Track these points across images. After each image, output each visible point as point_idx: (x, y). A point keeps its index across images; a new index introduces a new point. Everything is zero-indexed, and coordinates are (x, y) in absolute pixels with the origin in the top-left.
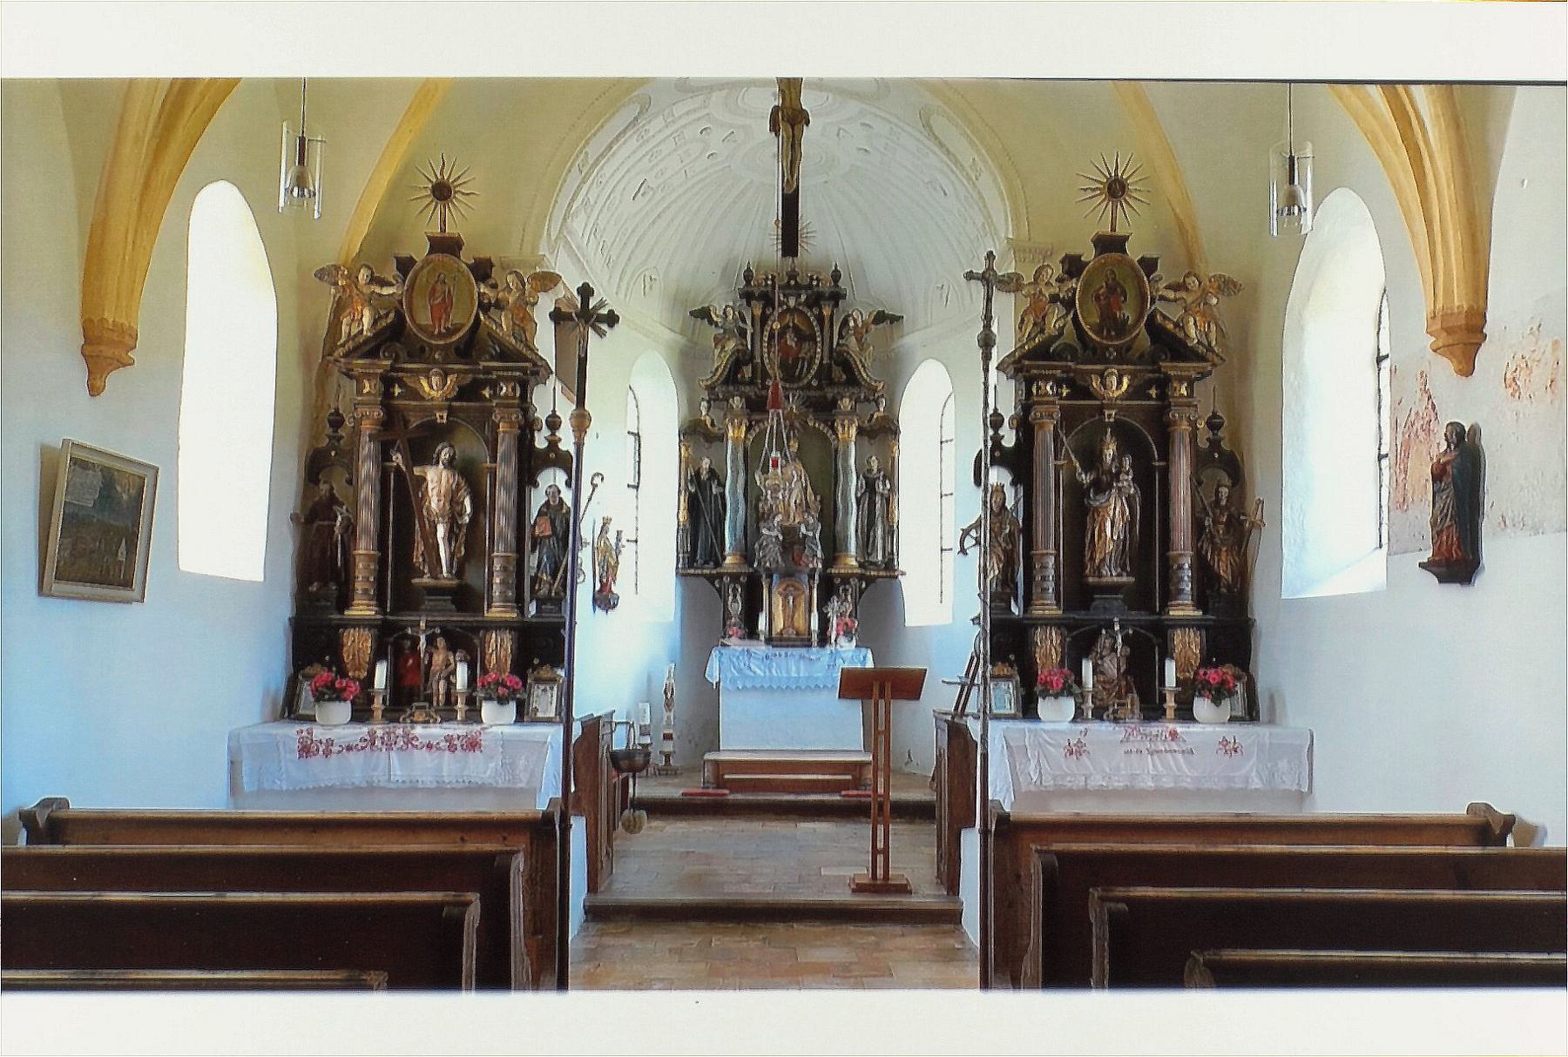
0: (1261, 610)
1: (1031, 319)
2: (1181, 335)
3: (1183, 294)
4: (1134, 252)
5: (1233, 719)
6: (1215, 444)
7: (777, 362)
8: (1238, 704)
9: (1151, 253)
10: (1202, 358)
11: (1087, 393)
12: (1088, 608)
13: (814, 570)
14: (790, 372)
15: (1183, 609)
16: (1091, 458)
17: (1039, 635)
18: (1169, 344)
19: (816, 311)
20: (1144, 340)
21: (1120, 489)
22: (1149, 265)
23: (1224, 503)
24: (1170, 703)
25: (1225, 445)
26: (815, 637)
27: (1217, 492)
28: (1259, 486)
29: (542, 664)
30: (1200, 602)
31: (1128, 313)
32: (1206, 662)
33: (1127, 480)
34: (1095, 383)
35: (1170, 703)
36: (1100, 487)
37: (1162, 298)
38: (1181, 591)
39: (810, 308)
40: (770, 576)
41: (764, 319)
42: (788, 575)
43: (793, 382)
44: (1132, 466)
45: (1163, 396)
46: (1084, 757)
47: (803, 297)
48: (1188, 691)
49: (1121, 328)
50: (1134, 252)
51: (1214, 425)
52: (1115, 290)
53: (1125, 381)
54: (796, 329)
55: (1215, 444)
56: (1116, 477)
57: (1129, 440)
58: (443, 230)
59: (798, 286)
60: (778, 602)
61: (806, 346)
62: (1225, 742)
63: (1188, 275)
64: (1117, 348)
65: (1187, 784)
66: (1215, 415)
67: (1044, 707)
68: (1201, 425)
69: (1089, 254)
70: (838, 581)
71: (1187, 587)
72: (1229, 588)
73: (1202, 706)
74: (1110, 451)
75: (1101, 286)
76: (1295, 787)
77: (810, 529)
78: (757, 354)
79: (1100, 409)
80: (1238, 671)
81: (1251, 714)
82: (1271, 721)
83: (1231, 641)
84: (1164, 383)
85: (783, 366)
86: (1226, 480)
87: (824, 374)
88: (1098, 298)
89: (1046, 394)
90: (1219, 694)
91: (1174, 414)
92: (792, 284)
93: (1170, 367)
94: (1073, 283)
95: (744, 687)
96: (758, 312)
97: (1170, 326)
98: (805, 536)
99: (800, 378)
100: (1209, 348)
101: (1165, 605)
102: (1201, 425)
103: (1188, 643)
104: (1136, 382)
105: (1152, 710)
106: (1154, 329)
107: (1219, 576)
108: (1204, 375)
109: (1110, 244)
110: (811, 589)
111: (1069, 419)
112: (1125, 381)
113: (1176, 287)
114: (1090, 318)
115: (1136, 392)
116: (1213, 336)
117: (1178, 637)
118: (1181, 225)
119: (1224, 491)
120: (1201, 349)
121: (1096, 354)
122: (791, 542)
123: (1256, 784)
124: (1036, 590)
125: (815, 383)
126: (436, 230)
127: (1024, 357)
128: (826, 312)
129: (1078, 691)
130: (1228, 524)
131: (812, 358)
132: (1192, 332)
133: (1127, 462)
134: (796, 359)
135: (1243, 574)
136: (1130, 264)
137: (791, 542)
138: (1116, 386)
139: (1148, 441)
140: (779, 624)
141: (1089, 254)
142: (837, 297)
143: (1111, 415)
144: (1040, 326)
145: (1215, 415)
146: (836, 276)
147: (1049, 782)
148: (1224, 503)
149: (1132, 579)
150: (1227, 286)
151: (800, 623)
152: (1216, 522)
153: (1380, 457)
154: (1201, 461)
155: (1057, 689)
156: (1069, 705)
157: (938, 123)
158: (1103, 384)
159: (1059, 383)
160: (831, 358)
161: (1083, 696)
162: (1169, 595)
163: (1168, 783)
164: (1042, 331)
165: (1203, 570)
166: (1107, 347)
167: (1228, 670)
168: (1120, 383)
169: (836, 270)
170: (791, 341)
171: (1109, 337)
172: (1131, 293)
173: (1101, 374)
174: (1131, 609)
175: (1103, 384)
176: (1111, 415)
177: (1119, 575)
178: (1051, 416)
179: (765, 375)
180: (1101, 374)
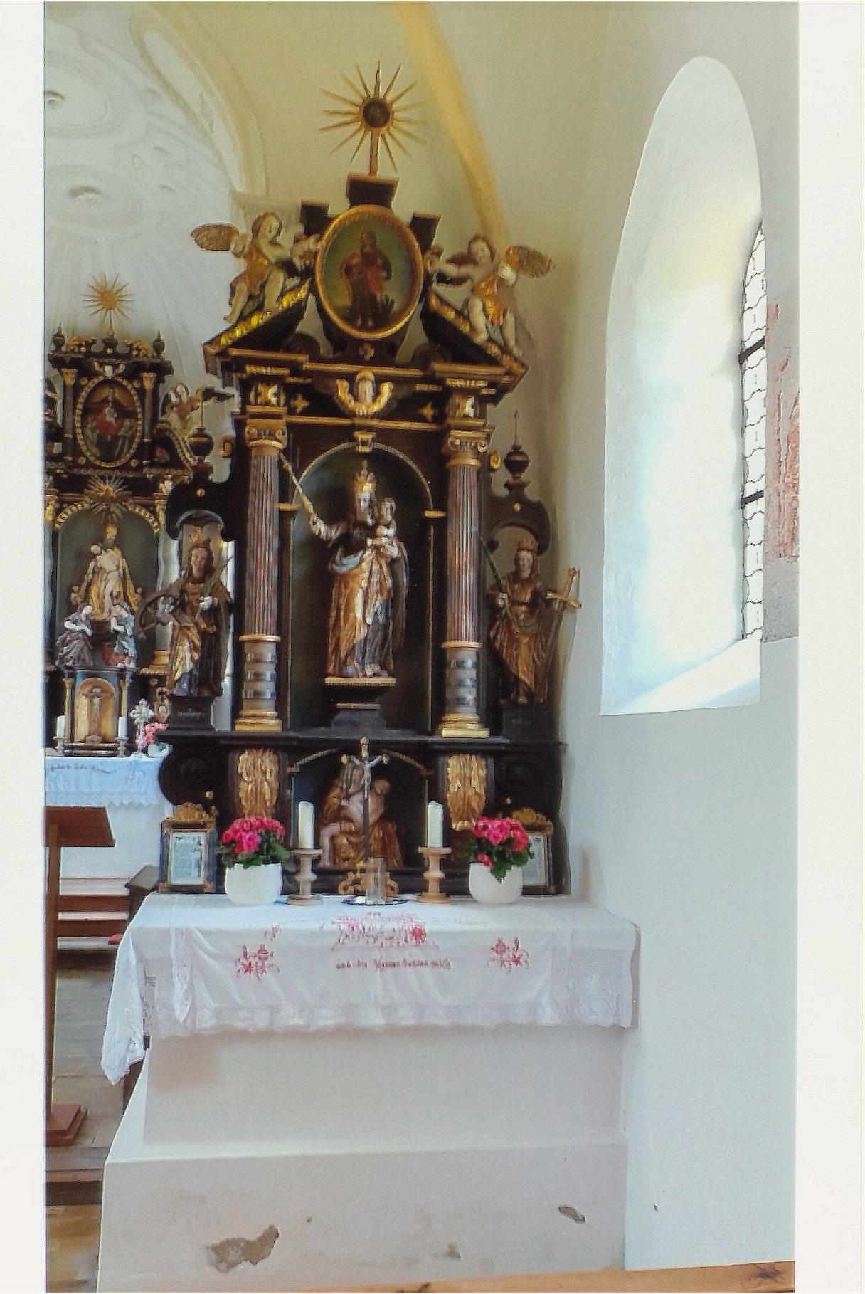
0: (576, 729)
1: (243, 288)
2: (466, 328)
3: (466, 270)
4: (403, 207)
5: (528, 891)
6: (516, 489)
7: (92, 436)
8: (536, 869)
9: (426, 210)
10: (493, 361)
11: (325, 404)
12: (328, 725)
13: (123, 670)
14: (108, 449)
15: (464, 725)
16: (336, 503)
17: (245, 762)
18: (449, 340)
19: (137, 385)
20: (417, 336)
21: (377, 549)
22: (423, 226)
23: (526, 574)
24: (434, 873)
25: (531, 493)
26: (121, 748)
27: (517, 560)
28: (573, 551)
29: (517, 806)
30: (491, 717)
31: (391, 291)
32: (491, 811)
33: (387, 533)
34: (342, 389)
35: (434, 873)
36: (351, 545)
37: (442, 278)
38: (460, 701)
39: (130, 379)
40: (73, 676)
41: (77, 388)
42: (92, 673)
43: (108, 461)
44: (396, 516)
45: (440, 418)
46: (268, 977)
47: (122, 368)
48: (462, 849)
49: (382, 316)
50: (403, 207)
51: (515, 464)
52: (373, 260)
53: (386, 389)
54: (116, 404)
55: (516, 489)
56: (371, 532)
57: (394, 481)
58: (373, 170)
59: (115, 355)
60: (82, 703)
61: (127, 422)
62: (500, 947)
63: (476, 238)
64: (376, 344)
65: (441, 1019)
66: (516, 449)
67: (234, 875)
68: (497, 464)
69: (339, 208)
70: (154, 682)
71: (469, 695)
72: (530, 695)
73: (479, 875)
74: (365, 490)
75: (352, 252)
76: (610, 1021)
77: (121, 620)
78: (69, 426)
79: (347, 433)
80: (540, 819)
81: (557, 881)
82: (584, 898)
83: (530, 772)
84: (442, 399)
85: (101, 443)
86: (529, 540)
87: (145, 452)
88: (348, 271)
89: (267, 403)
90: (504, 857)
91: (456, 437)
92: (109, 348)
93: (456, 374)
94: (311, 243)
95: (121, 804)
96: (70, 381)
97: (451, 315)
98: (117, 632)
99: (118, 458)
100: (505, 349)
101: (438, 721)
102: (497, 464)
103: (466, 779)
104: (400, 395)
105: (407, 879)
106: (431, 320)
107: (517, 680)
108: (500, 391)
109: (368, 192)
110: (121, 692)
111: (303, 444)
112: (386, 389)
113: (458, 260)
114: (338, 298)
115: (402, 407)
116: (510, 332)
117: (454, 767)
118: (470, 177)
119: (526, 556)
120: (494, 350)
121: (345, 348)
122: (101, 637)
123: (548, 1016)
124: (247, 692)
125: (134, 463)
126: (362, 170)
127: (238, 343)
128: (148, 385)
129: (285, 854)
130: (533, 605)
131: (133, 437)
132: (480, 321)
133: (388, 506)
134: (116, 438)
135: (550, 674)
136: (394, 225)
137: (101, 637)
138: (369, 397)
139: (417, 480)
140: (82, 729)
141: (339, 208)
142: (162, 370)
143: (365, 441)
144: (256, 302)
145: (516, 449)
146: (159, 346)
147: (207, 1021)
148: (526, 574)
149: (391, 681)
150: (530, 261)
151: (107, 729)
152: (514, 602)
153: (744, 501)
154: (494, 512)
155: (245, 853)
156: (270, 875)
157: (153, 40)
158: (353, 392)
159: (290, 391)
160: (152, 436)
161: (297, 861)
162: (442, 706)
163: (407, 1017)
164: (260, 308)
165: (496, 670)
166: (361, 342)
167: (527, 816)
168: (377, 393)
169: (159, 340)
170: (109, 415)
171: (363, 328)
172: (398, 265)
173: (350, 378)
174: (389, 726)
175: (353, 392)
176: (365, 441)
177: (376, 675)
178: (272, 436)
179: (77, 452)
180: (350, 378)
